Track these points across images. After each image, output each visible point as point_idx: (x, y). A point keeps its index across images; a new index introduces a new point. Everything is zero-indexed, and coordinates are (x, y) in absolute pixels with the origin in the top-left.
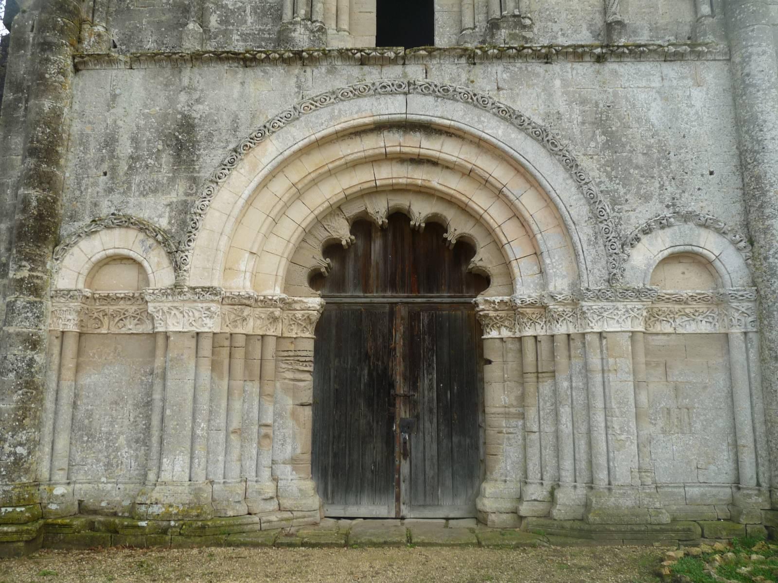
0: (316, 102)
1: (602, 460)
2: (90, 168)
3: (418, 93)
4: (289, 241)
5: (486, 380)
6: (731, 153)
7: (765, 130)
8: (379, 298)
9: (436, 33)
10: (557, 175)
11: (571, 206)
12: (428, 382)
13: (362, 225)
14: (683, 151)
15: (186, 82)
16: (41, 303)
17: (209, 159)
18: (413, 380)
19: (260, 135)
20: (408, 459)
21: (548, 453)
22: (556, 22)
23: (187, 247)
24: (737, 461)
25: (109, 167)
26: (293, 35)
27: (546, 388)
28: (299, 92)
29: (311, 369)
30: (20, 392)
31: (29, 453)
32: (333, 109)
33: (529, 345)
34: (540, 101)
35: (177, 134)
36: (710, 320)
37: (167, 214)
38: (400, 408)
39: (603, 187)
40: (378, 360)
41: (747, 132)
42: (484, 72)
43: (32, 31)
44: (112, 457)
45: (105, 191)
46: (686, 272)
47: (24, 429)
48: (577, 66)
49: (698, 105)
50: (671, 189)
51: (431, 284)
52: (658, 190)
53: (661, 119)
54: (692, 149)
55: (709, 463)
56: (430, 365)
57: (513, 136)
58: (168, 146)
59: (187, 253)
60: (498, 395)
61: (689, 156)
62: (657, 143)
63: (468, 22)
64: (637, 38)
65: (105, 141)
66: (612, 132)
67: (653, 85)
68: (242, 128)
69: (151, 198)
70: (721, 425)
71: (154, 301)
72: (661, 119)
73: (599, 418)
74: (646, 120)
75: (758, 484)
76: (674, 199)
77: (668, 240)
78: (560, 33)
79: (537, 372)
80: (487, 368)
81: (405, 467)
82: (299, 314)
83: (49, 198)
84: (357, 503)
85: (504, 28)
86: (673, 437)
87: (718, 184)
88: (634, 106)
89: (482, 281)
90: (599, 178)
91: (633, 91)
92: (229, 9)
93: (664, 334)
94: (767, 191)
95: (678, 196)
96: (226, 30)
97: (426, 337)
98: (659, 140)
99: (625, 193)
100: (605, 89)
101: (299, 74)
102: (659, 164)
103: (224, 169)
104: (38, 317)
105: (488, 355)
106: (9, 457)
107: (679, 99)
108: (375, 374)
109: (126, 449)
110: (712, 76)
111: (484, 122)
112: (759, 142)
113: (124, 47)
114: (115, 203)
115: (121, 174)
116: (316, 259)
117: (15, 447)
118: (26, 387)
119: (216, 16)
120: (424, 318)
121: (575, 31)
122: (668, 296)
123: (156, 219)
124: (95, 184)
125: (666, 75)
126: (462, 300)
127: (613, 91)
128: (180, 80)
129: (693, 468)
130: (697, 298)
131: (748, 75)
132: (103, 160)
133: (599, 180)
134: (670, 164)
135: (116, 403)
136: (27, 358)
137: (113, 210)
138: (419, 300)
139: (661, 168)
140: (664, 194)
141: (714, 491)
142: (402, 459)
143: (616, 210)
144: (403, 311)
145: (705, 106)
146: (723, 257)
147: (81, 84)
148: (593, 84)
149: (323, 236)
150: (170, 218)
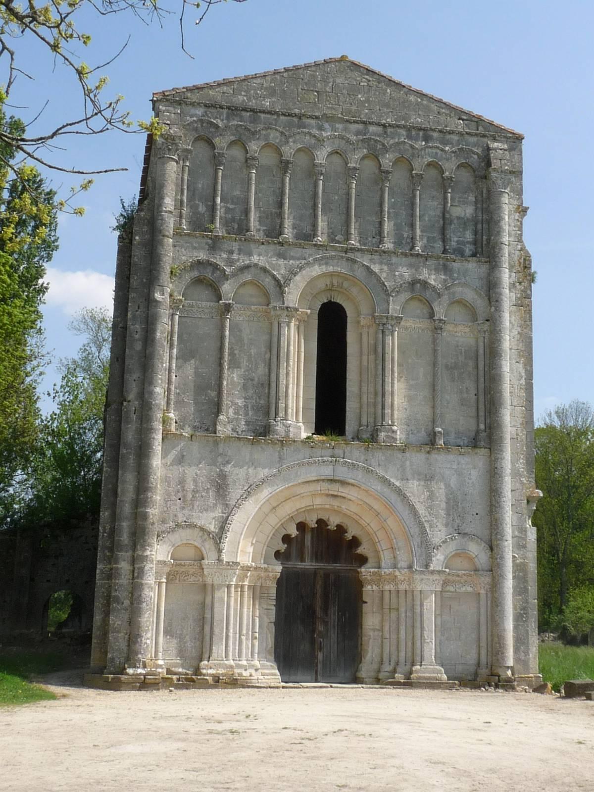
1: (418, 652)
5: (363, 611)
8: (308, 565)
9: (347, 424)
12: (333, 612)
13: (301, 526)
15: (221, 451)
17: (235, 493)
18: (326, 610)
21: (394, 648)
24: (479, 654)
26: (276, 428)
27: (394, 615)
29: (275, 603)
32: (297, 471)
36: (472, 586)
37: (213, 523)
39: (426, 519)
41: (494, 496)
43: (135, 413)
45: (180, 508)
48: (418, 454)
49: (474, 478)
50: (458, 521)
57: (385, 490)
60: (371, 621)
63: (364, 422)
68: (251, 479)
69: (205, 513)
71: (207, 568)
73: (418, 632)
75: (487, 664)
79: (390, 609)
80: (364, 605)
81: (320, 656)
82: (271, 574)
89: (363, 560)
96: (238, 418)
102: (453, 508)
105: (365, 599)
112: (498, 503)
113: (181, 424)
114: (186, 515)
115: (189, 499)
120: (332, 577)
123: (207, 525)
126: (352, 568)
131: (496, 468)
132: (178, 492)
135: (184, 619)
137: (185, 519)
144: (322, 572)
146: (479, 556)
149: (284, 532)
150: (215, 525)
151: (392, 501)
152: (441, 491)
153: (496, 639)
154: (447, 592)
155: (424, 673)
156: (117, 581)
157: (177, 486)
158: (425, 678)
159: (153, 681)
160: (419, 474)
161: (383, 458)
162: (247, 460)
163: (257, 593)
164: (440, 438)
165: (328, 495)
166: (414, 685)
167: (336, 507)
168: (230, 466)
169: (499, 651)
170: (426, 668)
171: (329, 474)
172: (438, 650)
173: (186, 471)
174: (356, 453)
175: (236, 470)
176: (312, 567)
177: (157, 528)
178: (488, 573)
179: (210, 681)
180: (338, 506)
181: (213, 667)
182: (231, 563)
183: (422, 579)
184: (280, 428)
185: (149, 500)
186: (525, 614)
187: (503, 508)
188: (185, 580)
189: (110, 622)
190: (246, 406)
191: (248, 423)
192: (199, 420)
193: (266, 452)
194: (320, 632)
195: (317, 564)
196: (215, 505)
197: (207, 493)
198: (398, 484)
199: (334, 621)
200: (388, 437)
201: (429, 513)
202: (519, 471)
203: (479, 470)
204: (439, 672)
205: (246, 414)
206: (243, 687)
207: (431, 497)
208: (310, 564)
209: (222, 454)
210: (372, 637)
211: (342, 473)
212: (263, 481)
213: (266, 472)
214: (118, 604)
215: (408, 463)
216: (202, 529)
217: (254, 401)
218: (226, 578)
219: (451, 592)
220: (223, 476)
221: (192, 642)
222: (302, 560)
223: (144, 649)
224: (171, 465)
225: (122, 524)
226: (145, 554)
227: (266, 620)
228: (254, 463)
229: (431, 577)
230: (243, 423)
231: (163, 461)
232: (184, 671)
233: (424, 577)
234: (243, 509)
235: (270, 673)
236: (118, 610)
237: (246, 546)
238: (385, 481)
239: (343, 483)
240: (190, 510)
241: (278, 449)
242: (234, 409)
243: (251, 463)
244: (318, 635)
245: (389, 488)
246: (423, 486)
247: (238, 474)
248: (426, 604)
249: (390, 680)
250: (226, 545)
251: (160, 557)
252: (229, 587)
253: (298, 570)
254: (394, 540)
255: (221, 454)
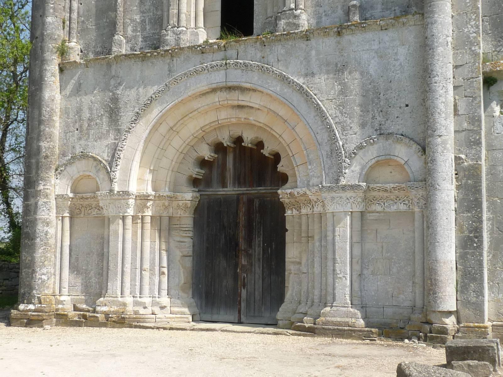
0: (177, 80)
2: (70, 126)
3: (232, 68)
4: (172, 161)
6: (421, 90)
7: (432, 77)
8: (231, 190)
10: (310, 114)
11: (317, 133)
12: (258, 241)
13: (219, 148)
14: (389, 92)
15: (113, 73)
16: (50, 202)
17: (126, 116)
18: (250, 240)
19: (149, 102)
20: (246, 289)
22: (321, 6)
23: (116, 169)
25: (79, 125)
28: (169, 74)
30: (42, 248)
31: (48, 279)
32: (186, 83)
33: (304, 219)
34: (302, 66)
35: (110, 104)
36: (407, 202)
38: (242, 258)
39: (337, 120)
40: (230, 229)
42: (270, 50)
44: (88, 282)
45: (78, 139)
46: (393, 171)
47: (45, 267)
48: (326, 40)
49: (402, 58)
51: (260, 182)
52: (371, 119)
53: (377, 71)
54: (395, 90)
55: (400, 294)
56: (259, 232)
57: (285, 90)
58: (106, 111)
59: (115, 173)
60: (292, 252)
61: (393, 95)
62: (372, 88)
64: (373, 11)
65: (77, 111)
66: (345, 83)
67: (373, 47)
70: (409, 270)
72: (377, 71)
73: (330, 264)
74: (367, 73)
76: (380, 125)
77: (375, 152)
78: (324, 14)
81: (244, 293)
82: (181, 203)
83: (51, 146)
84: (217, 314)
85: (283, 19)
86: (379, 276)
87: (411, 113)
88: (359, 63)
89: (283, 179)
90: (335, 114)
91: (360, 53)
92: (137, 22)
93: (377, 212)
94: (430, 118)
95: (383, 123)
97: (258, 215)
98: (374, 86)
99: (350, 123)
100: (342, 54)
101: (170, 62)
103: (132, 124)
104: (49, 209)
105: (288, 227)
106: (39, 280)
107: (390, 56)
108: (228, 238)
109: (94, 279)
110: (413, 36)
111: (269, 83)
113: (86, 52)
114: (83, 146)
116: (195, 171)
117: (41, 275)
118: (45, 246)
119: (131, 27)
120: (257, 203)
121: (334, 11)
122: (378, 188)
124: (73, 136)
125: (382, 40)
127: (347, 55)
128: (111, 71)
129: (390, 296)
130: (397, 189)
132: (76, 122)
133: (335, 115)
134: (380, 102)
135: (89, 254)
136: (45, 231)
138: (253, 192)
139: (374, 104)
140: (374, 122)
141: (401, 311)
142: (242, 287)
143: (344, 134)
144: (245, 199)
145: (406, 59)
146: (410, 162)
147: (64, 79)
148: (335, 52)
149: (195, 155)
150: (108, 152)
151: (295, 103)
152: (354, 81)
153: (427, 273)
154: (373, 212)
155: (335, 317)
156: (28, 218)
157: (75, 116)
158: (334, 324)
159: (36, 318)
160: (328, 64)
161: (283, 51)
162: (138, 79)
163: (165, 226)
164: (354, 13)
165: (233, 107)
166: (317, 331)
167: (243, 120)
168: (122, 88)
169: (430, 290)
170: (337, 310)
171: (221, 81)
172: (356, 286)
173: (83, 100)
174: (251, 51)
175: (127, 92)
176: (234, 193)
177: (55, 161)
178: (421, 184)
179: (100, 319)
180: (245, 118)
181: (108, 304)
182: (121, 193)
183: (333, 198)
184: (170, 37)
185: (42, 133)
186: (476, 237)
187: (434, 91)
188: (89, 214)
189: (23, 258)
190: (143, 21)
191: (145, 39)
192: (100, 44)
193: (157, 68)
194: (243, 266)
195: (240, 189)
196: (108, 131)
197: (101, 120)
198: (300, 81)
199: (259, 254)
200: (288, 24)
201: (341, 113)
202: (469, 38)
203: (409, 47)
204: (354, 316)
205: (143, 29)
206: (131, 326)
207: (343, 92)
208: (232, 189)
209: (115, 76)
210: (293, 272)
211: (237, 77)
212: (151, 100)
213: (155, 88)
214: (29, 240)
215: (313, 53)
216: (95, 159)
217: (151, 14)
218: (120, 209)
219: (377, 212)
220: (115, 100)
221: (96, 277)
222: (224, 185)
223: (38, 285)
224: (70, 96)
225: (31, 161)
226: (39, 189)
227: (178, 254)
228: (144, 82)
229: (344, 195)
230: (140, 39)
231: (63, 93)
232: (87, 307)
233: (334, 194)
234: (134, 133)
235: (182, 313)
236: (29, 245)
237: (142, 172)
238: (284, 79)
239: (242, 90)
240: (87, 140)
241: (168, 61)
242: (133, 27)
243: (141, 82)
244: (241, 270)
245: (290, 87)
246: (334, 78)
247: (130, 97)
248: (338, 230)
249: (299, 324)
250: (118, 174)
251: (59, 191)
252: (124, 218)
253: (219, 197)
254: (305, 152)
255: (113, 77)
